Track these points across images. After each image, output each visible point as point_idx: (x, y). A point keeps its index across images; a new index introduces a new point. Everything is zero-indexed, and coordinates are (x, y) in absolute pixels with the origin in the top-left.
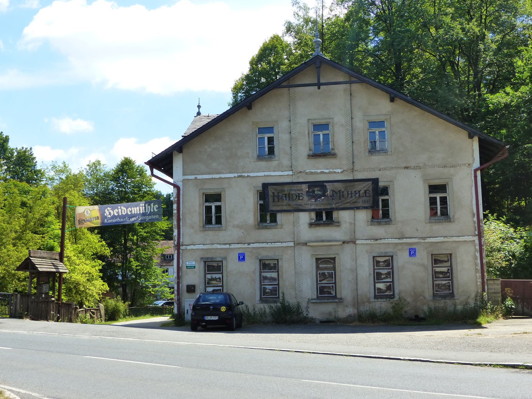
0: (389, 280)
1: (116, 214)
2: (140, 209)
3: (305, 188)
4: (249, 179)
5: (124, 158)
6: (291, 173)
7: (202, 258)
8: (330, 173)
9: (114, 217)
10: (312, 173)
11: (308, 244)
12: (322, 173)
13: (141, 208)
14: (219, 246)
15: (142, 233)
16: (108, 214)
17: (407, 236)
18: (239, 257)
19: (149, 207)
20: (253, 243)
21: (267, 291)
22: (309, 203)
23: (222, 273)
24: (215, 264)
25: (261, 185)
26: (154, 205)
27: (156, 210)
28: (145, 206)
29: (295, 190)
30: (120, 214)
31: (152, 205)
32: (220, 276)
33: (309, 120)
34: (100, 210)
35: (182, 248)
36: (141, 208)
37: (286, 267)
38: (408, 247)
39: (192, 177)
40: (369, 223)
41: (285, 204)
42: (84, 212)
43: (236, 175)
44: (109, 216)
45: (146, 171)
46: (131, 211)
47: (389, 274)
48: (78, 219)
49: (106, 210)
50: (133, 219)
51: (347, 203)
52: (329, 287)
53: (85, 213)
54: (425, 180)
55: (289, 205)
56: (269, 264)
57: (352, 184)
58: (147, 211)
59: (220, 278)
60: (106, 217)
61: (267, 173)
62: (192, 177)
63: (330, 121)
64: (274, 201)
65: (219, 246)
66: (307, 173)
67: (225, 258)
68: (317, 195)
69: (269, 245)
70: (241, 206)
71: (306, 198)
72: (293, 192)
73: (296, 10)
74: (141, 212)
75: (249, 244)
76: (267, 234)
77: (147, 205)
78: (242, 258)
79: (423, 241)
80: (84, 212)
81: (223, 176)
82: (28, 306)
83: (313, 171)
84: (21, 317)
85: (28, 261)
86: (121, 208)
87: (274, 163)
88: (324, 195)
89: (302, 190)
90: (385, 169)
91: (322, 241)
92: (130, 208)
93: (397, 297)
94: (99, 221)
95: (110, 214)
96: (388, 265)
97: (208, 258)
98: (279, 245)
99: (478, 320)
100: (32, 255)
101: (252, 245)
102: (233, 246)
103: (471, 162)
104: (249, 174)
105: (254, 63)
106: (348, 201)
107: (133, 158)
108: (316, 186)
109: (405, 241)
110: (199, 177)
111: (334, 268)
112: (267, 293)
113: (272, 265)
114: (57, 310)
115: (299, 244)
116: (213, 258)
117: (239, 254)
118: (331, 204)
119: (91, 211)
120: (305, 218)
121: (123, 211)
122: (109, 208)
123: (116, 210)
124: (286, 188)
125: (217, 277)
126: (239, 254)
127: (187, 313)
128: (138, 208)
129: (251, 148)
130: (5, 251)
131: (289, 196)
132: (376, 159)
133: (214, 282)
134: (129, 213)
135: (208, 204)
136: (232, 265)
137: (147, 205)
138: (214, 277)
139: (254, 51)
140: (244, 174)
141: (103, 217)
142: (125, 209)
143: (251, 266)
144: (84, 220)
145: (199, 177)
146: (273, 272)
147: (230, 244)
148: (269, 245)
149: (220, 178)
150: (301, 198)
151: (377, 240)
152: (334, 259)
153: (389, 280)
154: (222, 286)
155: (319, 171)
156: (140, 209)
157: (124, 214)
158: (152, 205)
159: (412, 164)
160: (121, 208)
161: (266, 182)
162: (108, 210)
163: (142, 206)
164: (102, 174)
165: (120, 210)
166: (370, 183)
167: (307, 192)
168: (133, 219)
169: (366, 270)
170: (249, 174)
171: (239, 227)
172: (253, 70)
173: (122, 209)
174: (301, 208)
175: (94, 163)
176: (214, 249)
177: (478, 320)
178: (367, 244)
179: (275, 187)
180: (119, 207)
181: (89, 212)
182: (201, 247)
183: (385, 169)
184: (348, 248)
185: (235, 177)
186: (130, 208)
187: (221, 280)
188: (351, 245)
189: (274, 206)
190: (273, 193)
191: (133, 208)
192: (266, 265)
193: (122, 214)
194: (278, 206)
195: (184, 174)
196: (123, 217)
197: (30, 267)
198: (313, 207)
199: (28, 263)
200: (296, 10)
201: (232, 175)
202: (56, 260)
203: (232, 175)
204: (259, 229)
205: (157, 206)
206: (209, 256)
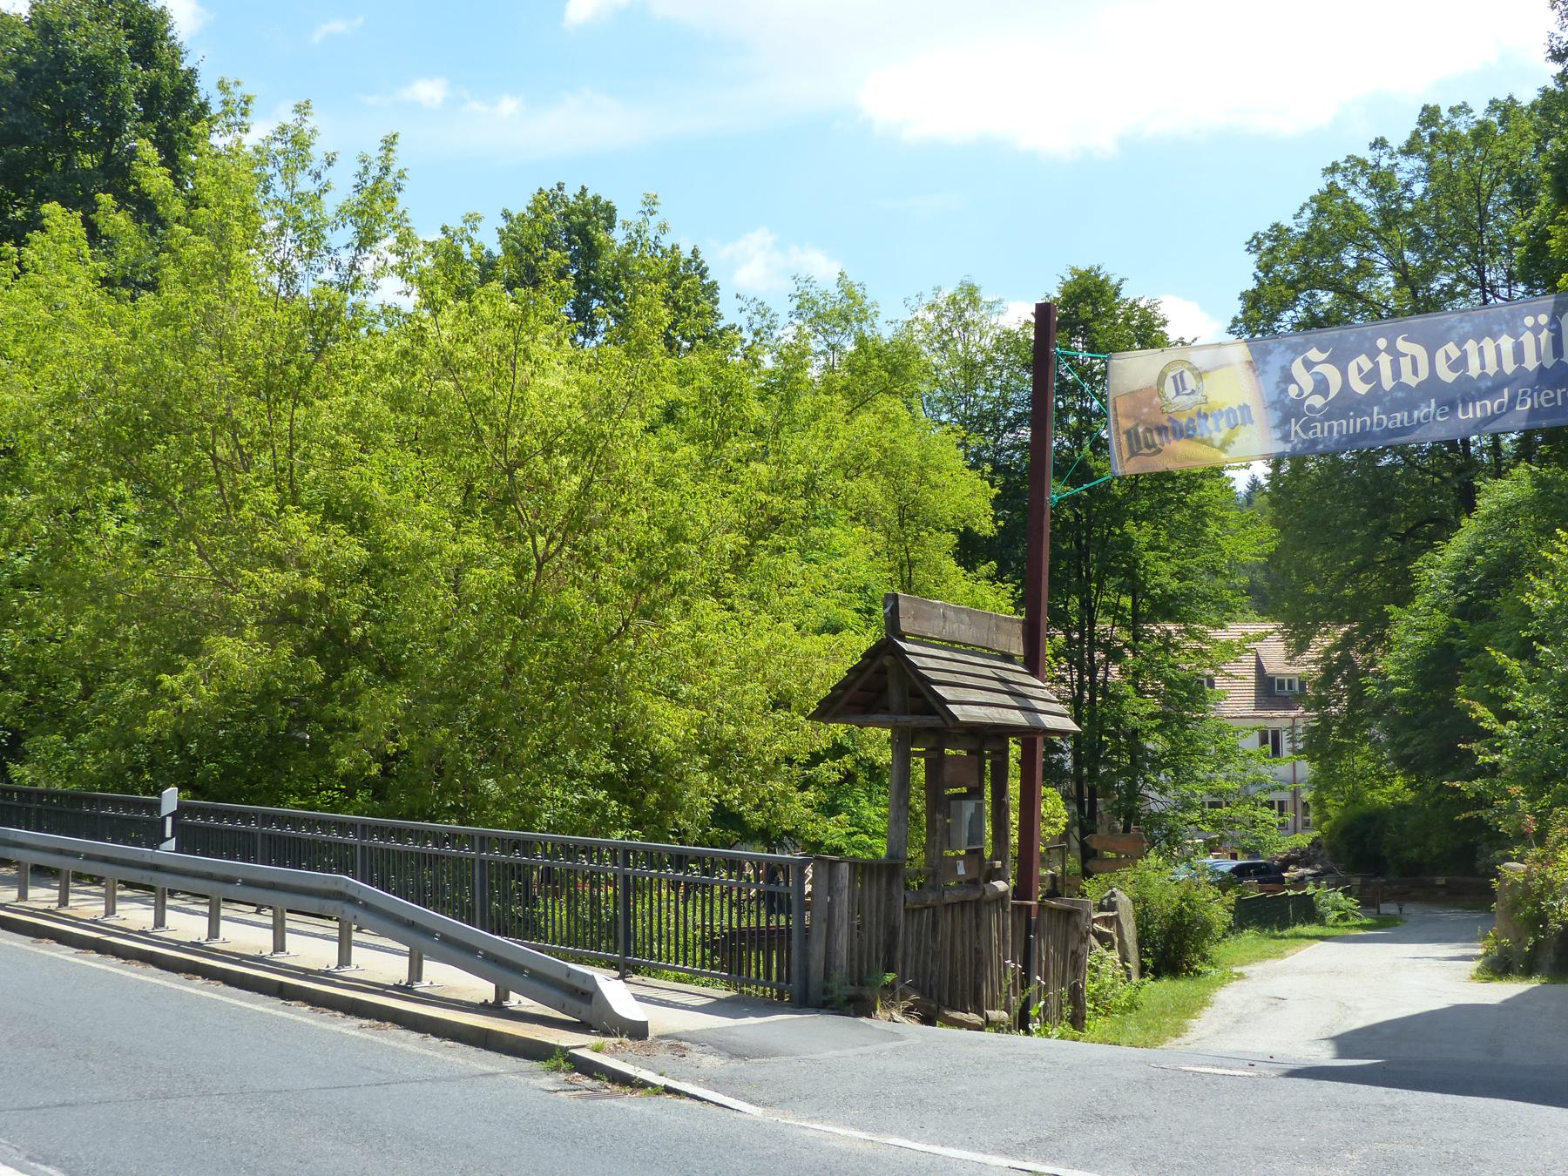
5: (1074, 271)
9: (1346, 404)
15: (1165, 580)
30: (1388, 383)
44: (1317, 401)
45: (1165, 323)
46: (1460, 364)
50: (1475, 411)
74: (1531, 364)
82: (892, 932)
84: (858, 1006)
85: (887, 661)
92: (1452, 349)
95: (1321, 386)
100: (905, 625)
107: (1112, 271)
114: (1021, 947)
121: (1405, 364)
122: (1314, 355)
130: (679, 627)
134: (1448, 376)
142: (1419, 351)
157: (1413, 382)
162: (1308, 365)
163: (1536, 329)
164: (987, 342)
165: (1384, 360)
168: (1475, 411)
173: (1396, 355)
175: (954, 301)
180: (1382, 343)
186: (1452, 349)
191: (1471, 346)
193: (1400, 386)
196: (1408, 398)
197: (895, 696)
199: (882, 671)
202: (1008, 658)
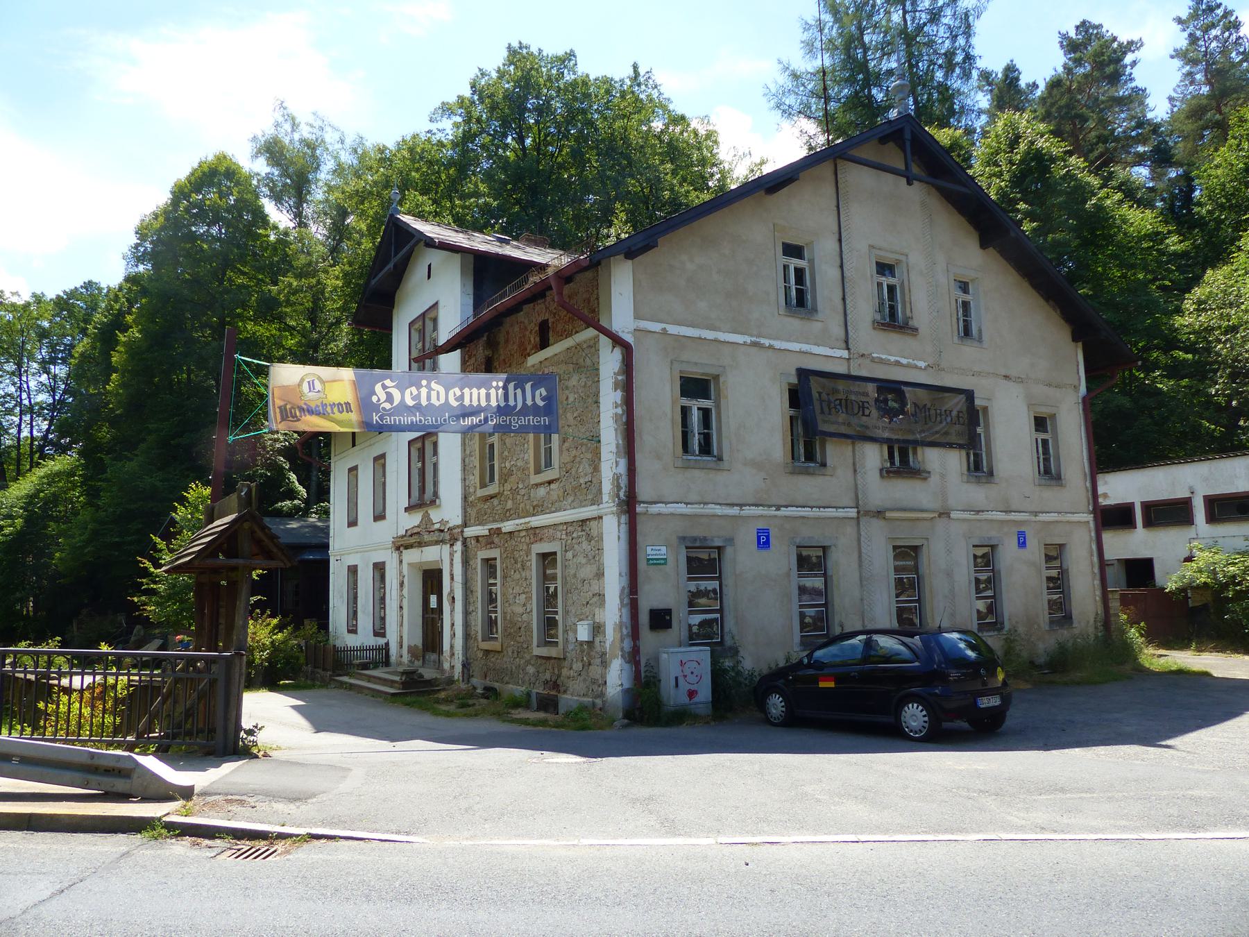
0: (989, 593)
1: (410, 403)
2: (488, 396)
3: (871, 388)
4: (770, 352)
6: (845, 354)
7: (683, 539)
8: (908, 366)
10: (881, 361)
11: (888, 514)
12: (898, 363)
13: (493, 391)
14: (719, 510)
16: (383, 397)
17: (1014, 508)
18: (759, 538)
19: (519, 391)
20: (786, 506)
21: (807, 620)
22: (880, 424)
23: (720, 578)
24: (704, 556)
25: (794, 372)
26: (534, 388)
27: (541, 404)
28: (505, 388)
29: (857, 393)
30: (424, 403)
31: (528, 386)
32: (716, 584)
33: (872, 247)
34: (356, 385)
35: (640, 509)
36: (493, 391)
37: (842, 563)
38: (1015, 530)
39: (656, 327)
40: (965, 478)
41: (840, 420)
42: (300, 384)
43: (748, 339)
44: (387, 406)
46: (462, 397)
47: (988, 581)
48: (279, 403)
49: (378, 388)
51: (937, 432)
52: (910, 609)
53: (305, 387)
54: (1030, 406)
55: (849, 424)
56: (809, 557)
57: (941, 395)
58: (511, 403)
59: (714, 591)
60: (376, 408)
61: (805, 347)
62: (656, 327)
63: (903, 258)
64: (822, 412)
65: (719, 510)
66: (873, 360)
67: (731, 541)
68: (892, 409)
69: (815, 513)
70: (755, 416)
71: (875, 413)
72: (853, 397)
73: (281, 119)
74: (494, 403)
75: (778, 508)
76: (809, 486)
77: (511, 386)
78: (764, 541)
79: (1033, 518)
80: (300, 384)
81: (722, 336)
83: (884, 357)
86: (428, 386)
87: (816, 326)
88: (903, 412)
89: (867, 395)
90: (979, 374)
91: (904, 510)
93: (1007, 626)
94: (354, 417)
95: (390, 398)
96: (987, 564)
97: (695, 539)
98: (831, 512)
99: (306, 622)
101: (784, 512)
102: (748, 511)
103: (1076, 383)
104: (772, 342)
105: (179, 193)
106: (937, 428)
108: (890, 391)
109: (1013, 516)
110: (673, 329)
111: (916, 569)
112: (807, 625)
113: (814, 559)
115: (867, 513)
116: (705, 539)
117: (759, 531)
118: (914, 434)
119: (323, 382)
120: (873, 456)
121: (434, 394)
123: (414, 389)
124: (841, 385)
125: (710, 588)
126: (759, 531)
127: (677, 685)
128: (483, 391)
129: (770, 283)
131: (846, 405)
132: (969, 351)
133: (703, 601)
135: (685, 402)
136: (744, 561)
137: (511, 386)
138: (702, 588)
139: (182, 171)
140: (763, 341)
141: (366, 404)
142: (442, 390)
143: (780, 559)
144: (301, 409)
145: (673, 329)
146: (816, 575)
147: (741, 505)
148: (815, 513)
149: (716, 340)
150: (867, 412)
151: (978, 512)
152: (916, 549)
153: (989, 593)
154: (721, 611)
155: (892, 359)
156: (488, 396)
157: (437, 404)
158: (528, 386)
159: (1013, 372)
160: (428, 386)
161: (804, 366)
162: (384, 387)
163: (497, 388)
165: (424, 391)
166: (962, 397)
167: (877, 400)
169: (964, 573)
170: (772, 342)
171: (757, 465)
172: (176, 201)
174: (869, 433)
176: (707, 516)
177: (306, 622)
178: (964, 520)
179: (822, 380)
180: (424, 382)
181: (318, 386)
182: (681, 509)
183: (979, 374)
184: (941, 524)
185: (745, 344)
187: (718, 595)
188: (944, 520)
189: (825, 422)
190: (820, 393)
191: (466, 391)
192: (811, 561)
194: (833, 423)
195: (637, 316)
198: (886, 435)
200: (281, 119)
201: (739, 339)
203: (739, 339)
204: (792, 473)
205: (543, 391)
206: (697, 532)
